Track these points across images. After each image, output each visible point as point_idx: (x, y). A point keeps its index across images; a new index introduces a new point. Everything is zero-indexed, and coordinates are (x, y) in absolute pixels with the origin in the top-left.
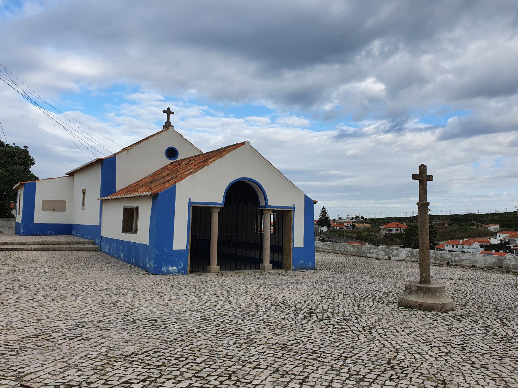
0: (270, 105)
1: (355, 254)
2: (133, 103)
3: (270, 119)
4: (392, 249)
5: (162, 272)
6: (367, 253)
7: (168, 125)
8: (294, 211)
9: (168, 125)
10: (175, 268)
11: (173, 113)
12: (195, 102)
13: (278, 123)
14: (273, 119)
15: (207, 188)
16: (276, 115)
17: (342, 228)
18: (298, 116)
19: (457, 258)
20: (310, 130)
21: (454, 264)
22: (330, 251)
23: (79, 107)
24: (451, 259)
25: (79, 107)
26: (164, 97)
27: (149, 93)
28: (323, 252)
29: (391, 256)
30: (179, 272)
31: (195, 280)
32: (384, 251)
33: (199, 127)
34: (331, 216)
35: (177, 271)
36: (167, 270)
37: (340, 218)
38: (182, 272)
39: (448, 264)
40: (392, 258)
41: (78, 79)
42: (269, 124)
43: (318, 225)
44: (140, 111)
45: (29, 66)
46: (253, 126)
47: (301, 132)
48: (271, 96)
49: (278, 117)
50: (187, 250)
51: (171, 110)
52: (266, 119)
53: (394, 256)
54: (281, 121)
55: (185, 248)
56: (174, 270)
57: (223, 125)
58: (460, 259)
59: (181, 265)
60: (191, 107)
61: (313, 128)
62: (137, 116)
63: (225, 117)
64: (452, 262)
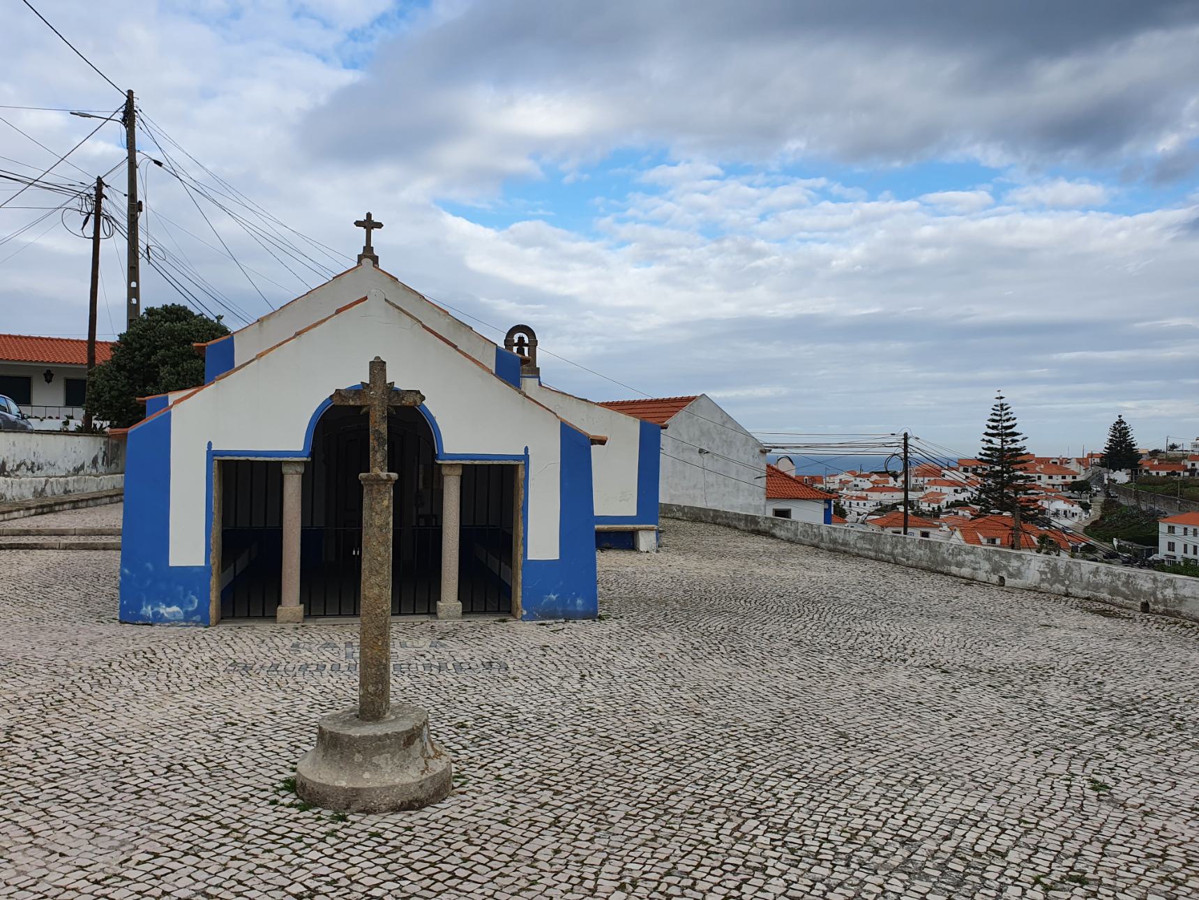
0: (993, 156)
1: (924, 564)
2: (654, 190)
3: (992, 194)
4: (1007, 557)
5: (142, 617)
6: (950, 564)
7: (368, 253)
8: (527, 466)
9: (368, 253)
10: (175, 609)
11: (379, 225)
12: (796, 171)
13: (1014, 203)
14: (998, 194)
15: (259, 411)
16: (1007, 180)
17: (1174, 473)
18: (1070, 179)
19: (1169, 592)
20: (1106, 214)
21: (1161, 608)
22: (872, 554)
23: (541, 212)
24: (1154, 594)
25: (541, 212)
26: (722, 167)
27: (689, 162)
28: (859, 555)
29: (1004, 574)
30: (188, 618)
31: (247, 641)
32: (989, 559)
33: (804, 230)
34: (1143, 442)
35: (181, 615)
36: (156, 614)
37: (1173, 447)
38: (199, 618)
39: (1145, 607)
40: (1009, 582)
41: (537, 147)
42: (987, 207)
43: (1102, 465)
44: (668, 206)
45: (443, 130)
46: (944, 215)
47: (1081, 221)
48: (1007, 133)
49: (1013, 186)
50: (206, 569)
51: (363, 218)
52: (979, 196)
53: (1011, 575)
54: (1022, 196)
55: (201, 562)
56: (174, 614)
57: (865, 220)
58: (1176, 598)
59: (191, 602)
60: (784, 184)
61: (1115, 208)
62: (661, 222)
63: (868, 201)
64: (1156, 602)
